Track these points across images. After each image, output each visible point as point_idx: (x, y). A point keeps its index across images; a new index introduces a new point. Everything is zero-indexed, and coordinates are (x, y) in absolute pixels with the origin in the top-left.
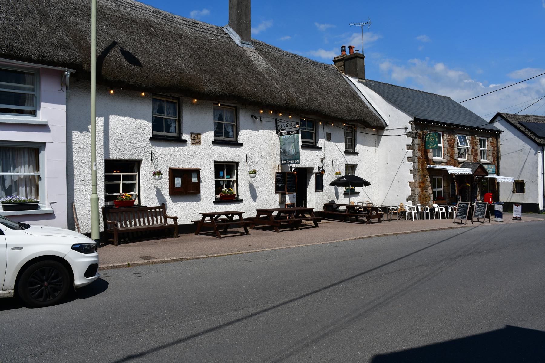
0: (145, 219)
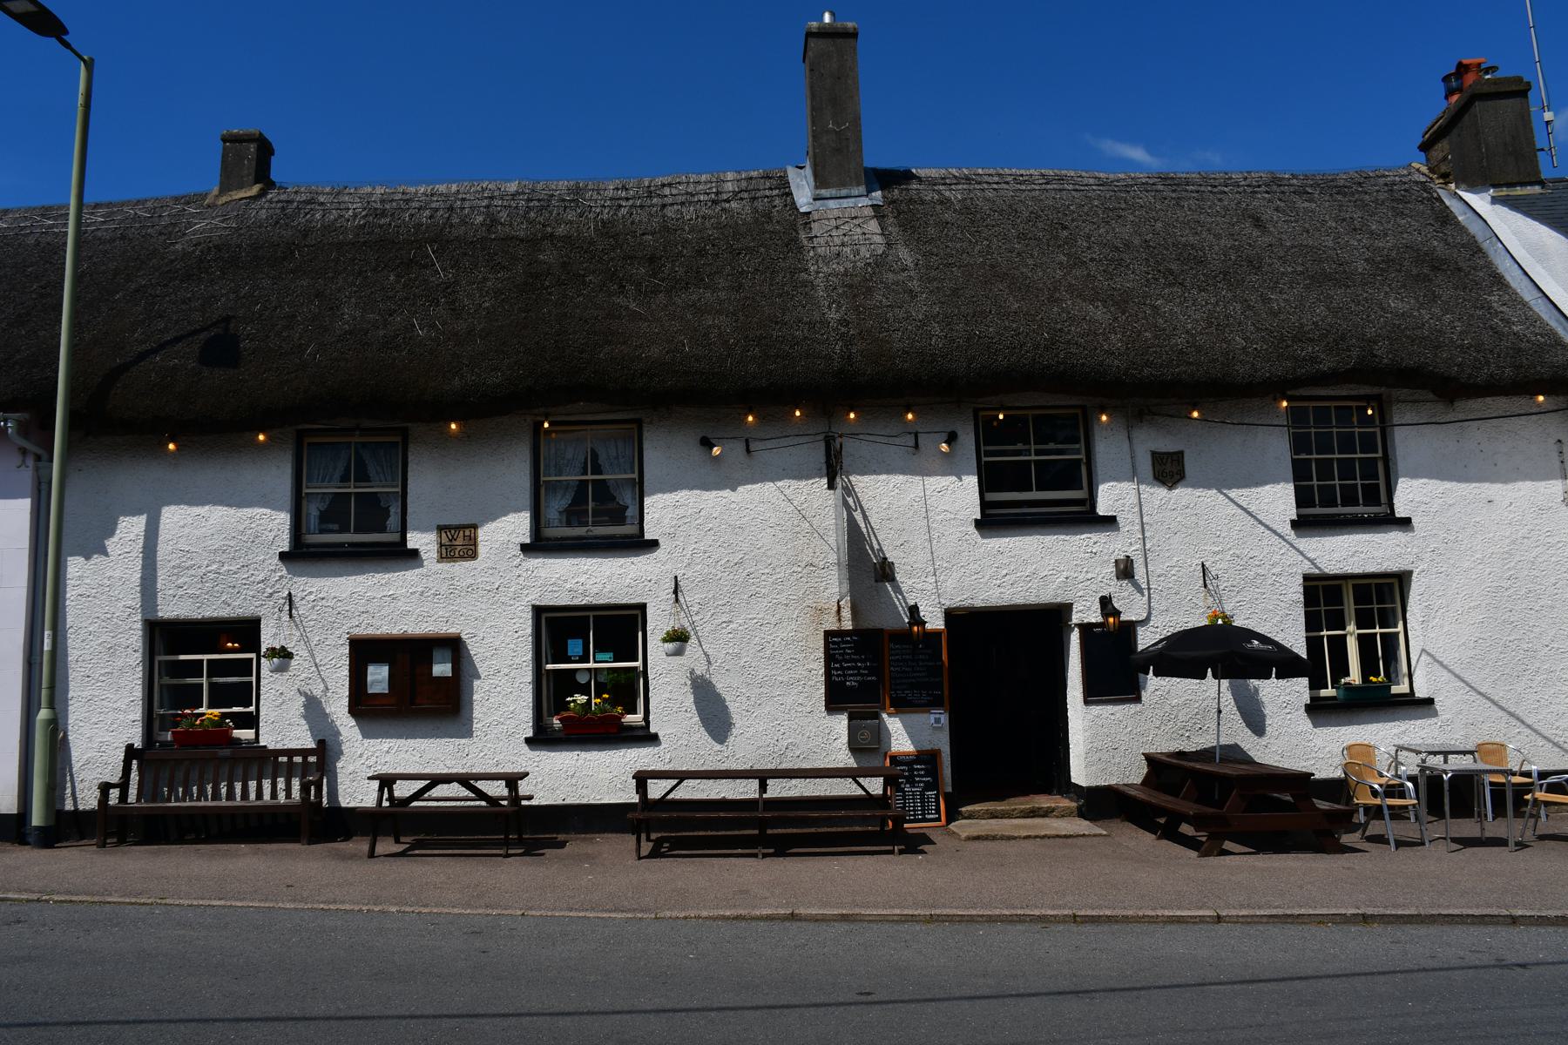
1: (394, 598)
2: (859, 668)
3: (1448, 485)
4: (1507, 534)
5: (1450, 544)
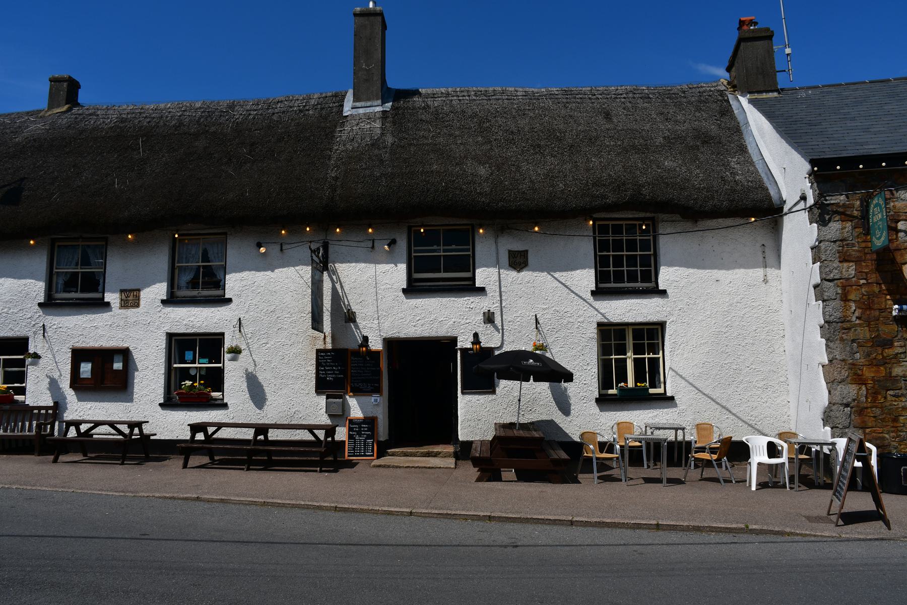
0: (139, 431)
1: (96, 328)
2: (334, 370)
3: (691, 271)
4: (727, 300)
5: (691, 306)
